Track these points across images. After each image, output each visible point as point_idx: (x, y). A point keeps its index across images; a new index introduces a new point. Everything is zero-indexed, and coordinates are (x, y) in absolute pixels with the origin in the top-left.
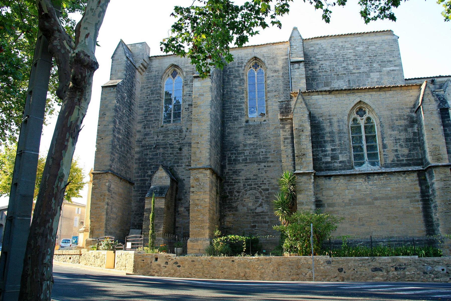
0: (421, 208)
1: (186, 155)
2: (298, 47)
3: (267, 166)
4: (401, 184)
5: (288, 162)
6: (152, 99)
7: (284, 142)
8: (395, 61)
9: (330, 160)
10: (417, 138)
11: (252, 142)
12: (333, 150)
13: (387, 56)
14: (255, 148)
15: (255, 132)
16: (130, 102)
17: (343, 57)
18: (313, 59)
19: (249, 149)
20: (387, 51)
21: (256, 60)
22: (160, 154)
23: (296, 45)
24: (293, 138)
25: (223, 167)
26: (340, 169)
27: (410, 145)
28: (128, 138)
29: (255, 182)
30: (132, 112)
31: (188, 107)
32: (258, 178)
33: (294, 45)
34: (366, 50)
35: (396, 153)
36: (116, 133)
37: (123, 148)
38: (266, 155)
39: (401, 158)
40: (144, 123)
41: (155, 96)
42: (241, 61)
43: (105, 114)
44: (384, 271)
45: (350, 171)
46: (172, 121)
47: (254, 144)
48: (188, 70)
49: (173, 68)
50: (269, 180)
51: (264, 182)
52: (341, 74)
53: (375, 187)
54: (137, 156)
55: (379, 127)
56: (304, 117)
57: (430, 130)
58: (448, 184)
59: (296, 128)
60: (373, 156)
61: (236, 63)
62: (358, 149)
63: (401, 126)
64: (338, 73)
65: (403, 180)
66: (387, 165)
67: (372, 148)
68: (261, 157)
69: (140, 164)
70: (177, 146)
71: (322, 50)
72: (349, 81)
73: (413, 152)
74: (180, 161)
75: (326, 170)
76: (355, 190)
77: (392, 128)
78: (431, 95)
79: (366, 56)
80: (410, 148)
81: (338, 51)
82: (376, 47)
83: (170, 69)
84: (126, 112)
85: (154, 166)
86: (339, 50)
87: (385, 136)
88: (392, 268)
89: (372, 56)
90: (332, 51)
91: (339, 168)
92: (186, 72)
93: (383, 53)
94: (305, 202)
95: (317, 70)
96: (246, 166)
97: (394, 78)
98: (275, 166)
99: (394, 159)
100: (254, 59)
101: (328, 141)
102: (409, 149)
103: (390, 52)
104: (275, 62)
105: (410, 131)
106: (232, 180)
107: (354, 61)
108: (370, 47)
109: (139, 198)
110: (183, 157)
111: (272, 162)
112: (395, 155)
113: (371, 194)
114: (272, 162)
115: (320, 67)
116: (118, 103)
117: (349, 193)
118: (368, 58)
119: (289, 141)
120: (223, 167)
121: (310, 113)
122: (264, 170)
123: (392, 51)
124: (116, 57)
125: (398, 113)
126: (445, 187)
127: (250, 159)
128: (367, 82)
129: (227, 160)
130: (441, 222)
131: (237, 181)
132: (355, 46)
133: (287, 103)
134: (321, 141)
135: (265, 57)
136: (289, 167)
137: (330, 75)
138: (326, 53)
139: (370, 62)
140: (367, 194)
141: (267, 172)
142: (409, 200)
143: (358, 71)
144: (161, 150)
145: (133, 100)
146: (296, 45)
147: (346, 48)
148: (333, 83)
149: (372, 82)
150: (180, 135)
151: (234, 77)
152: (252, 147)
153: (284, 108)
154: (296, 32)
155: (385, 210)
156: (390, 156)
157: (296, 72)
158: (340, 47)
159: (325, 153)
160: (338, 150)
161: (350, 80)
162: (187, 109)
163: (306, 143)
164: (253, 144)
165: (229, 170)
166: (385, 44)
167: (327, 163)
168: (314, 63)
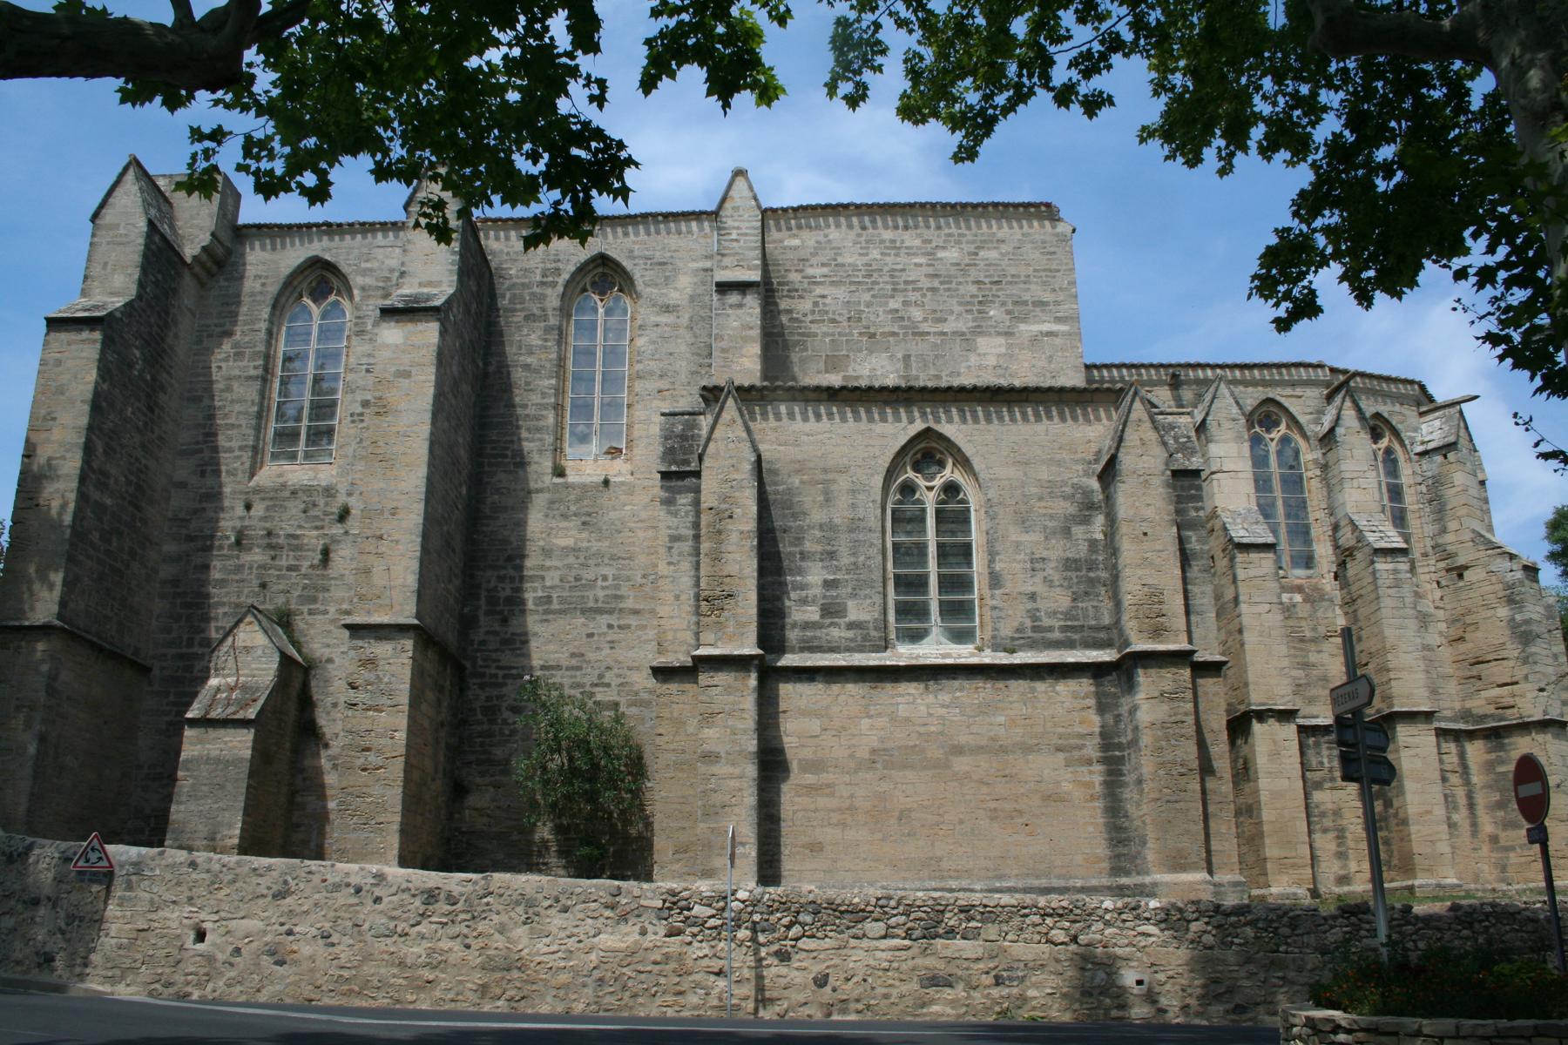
0: (1097, 784)
1: (343, 575)
2: (746, 235)
3: (620, 627)
4: (1039, 705)
5: (680, 617)
6: (237, 372)
7: (670, 548)
8: (1057, 303)
9: (816, 617)
10: (1101, 558)
11: (570, 542)
12: (828, 584)
13: (1033, 287)
14: (582, 565)
15: (583, 511)
16: (154, 379)
17: (892, 276)
18: (794, 277)
19: (559, 564)
20: (1035, 271)
21: (604, 264)
22: (251, 568)
23: (738, 228)
24: (697, 537)
25: (467, 623)
26: (848, 650)
27: (1075, 580)
28: (138, 508)
29: (575, 676)
30: (159, 417)
31: (360, 410)
32: (585, 666)
33: (734, 228)
34: (967, 261)
35: (1030, 605)
36: (92, 488)
37: (114, 539)
38: (617, 587)
39: (1046, 622)
40: (201, 455)
41: (245, 363)
42: (554, 265)
43: (54, 419)
44: (961, 986)
45: (879, 655)
46: (300, 455)
47: (579, 550)
48: (369, 281)
49: (318, 272)
50: (620, 672)
51: (606, 680)
52: (882, 334)
53: (957, 710)
54: (167, 571)
55: (983, 516)
56: (737, 470)
57: (1137, 537)
58: (1181, 710)
59: (711, 505)
60: (957, 610)
61: (538, 271)
62: (912, 584)
63: (1052, 517)
64: (872, 330)
65: (1046, 692)
66: (999, 641)
67: (955, 583)
68: (601, 594)
69: (178, 601)
70: (314, 541)
71: (828, 251)
72: (907, 358)
73: (1084, 605)
74: (321, 596)
75: (802, 650)
76: (893, 719)
77: (1023, 522)
78: (1148, 424)
79: (969, 279)
80: (1074, 589)
81: (879, 257)
82: (1001, 254)
83: (306, 273)
84: (133, 413)
85: (226, 609)
86: (882, 254)
87: (998, 547)
88: (984, 976)
89: (987, 280)
90: (860, 254)
91: (844, 643)
92: (363, 289)
93: (1023, 274)
94: (723, 754)
95: (805, 315)
96: (546, 620)
97: (1050, 359)
98: (643, 627)
99: (1022, 624)
100: (599, 261)
101: (814, 554)
102: (1074, 593)
103: (1043, 274)
104: (667, 278)
105: (1080, 536)
106: (499, 668)
107: (929, 294)
108: (981, 253)
109: (166, 718)
110: (333, 582)
111: (636, 612)
112: (1028, 611)
113: (942, 733)
114: (636, 612)
115: (816, 304)
116: (104, 381)
117: (872, 727)
118: (973, 289)
119: (686, 546)
120: (467, 623)
121: (759, 457)
122: (609, 639)
123: (1050, 271)
124: (109, 216)
125: (1044, 474)
126: (1173, 719)
127: (562, 600)
128: (964, 364)
129: (483, 602)
130: (1151, 835)
131: (514, 672)
132: (934, 245)
133: (687, 421)
134: (790, 553)
135: (634, 258)
136: (679, 635)
137: (846, 335)
138: (840, 260)
139: (980, 302)
140: (929, 734)
141: (616, 645)
142: (1061, 756)
143: (940, 327)
144: (257, 556)
145: (165, 375)
146: (738, 228)
147: (907, 248)
148: (855, 361)
149: (980, 367)
150: (327, 504)
151: (527, 318)
152: (571, 560)
153: (677, 436)
154: (740, 183)
155: (985, 789)
156: (1010, 612)
157: (733, 318)
158: (888, 244)
159: (804, 593)
160: (845, 587)
161: (909, 356)
162: (355, 418)
163: (737, 557)
164: (575, 550)
165: (488, 633)
166: (1030, 245)
167: (807, 625)
168: (797, 291)
